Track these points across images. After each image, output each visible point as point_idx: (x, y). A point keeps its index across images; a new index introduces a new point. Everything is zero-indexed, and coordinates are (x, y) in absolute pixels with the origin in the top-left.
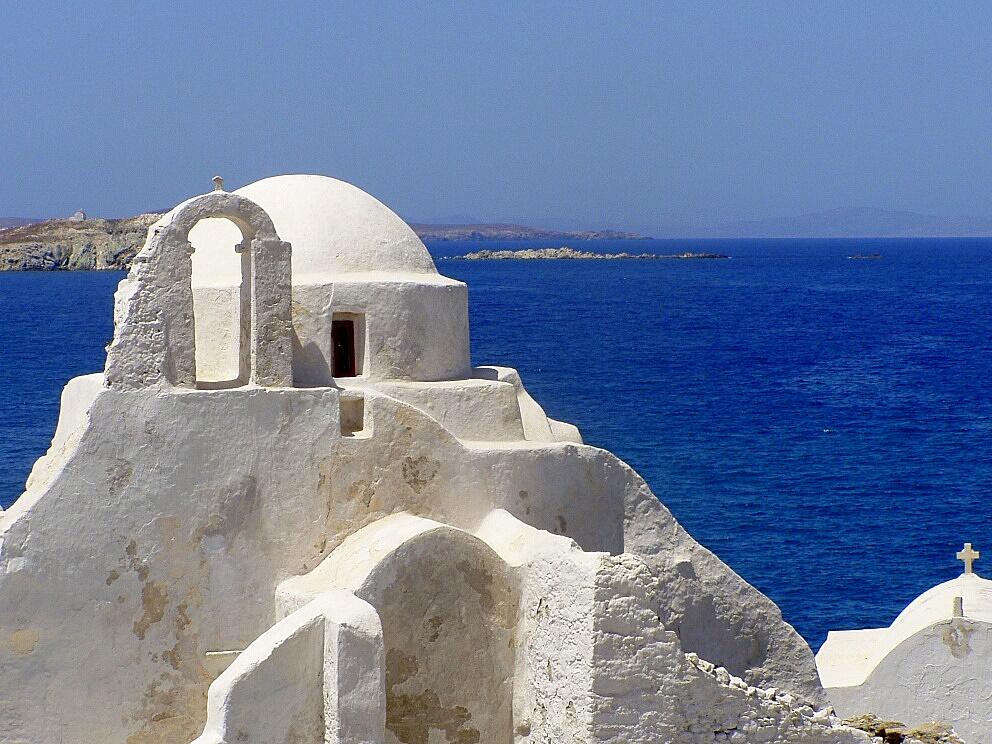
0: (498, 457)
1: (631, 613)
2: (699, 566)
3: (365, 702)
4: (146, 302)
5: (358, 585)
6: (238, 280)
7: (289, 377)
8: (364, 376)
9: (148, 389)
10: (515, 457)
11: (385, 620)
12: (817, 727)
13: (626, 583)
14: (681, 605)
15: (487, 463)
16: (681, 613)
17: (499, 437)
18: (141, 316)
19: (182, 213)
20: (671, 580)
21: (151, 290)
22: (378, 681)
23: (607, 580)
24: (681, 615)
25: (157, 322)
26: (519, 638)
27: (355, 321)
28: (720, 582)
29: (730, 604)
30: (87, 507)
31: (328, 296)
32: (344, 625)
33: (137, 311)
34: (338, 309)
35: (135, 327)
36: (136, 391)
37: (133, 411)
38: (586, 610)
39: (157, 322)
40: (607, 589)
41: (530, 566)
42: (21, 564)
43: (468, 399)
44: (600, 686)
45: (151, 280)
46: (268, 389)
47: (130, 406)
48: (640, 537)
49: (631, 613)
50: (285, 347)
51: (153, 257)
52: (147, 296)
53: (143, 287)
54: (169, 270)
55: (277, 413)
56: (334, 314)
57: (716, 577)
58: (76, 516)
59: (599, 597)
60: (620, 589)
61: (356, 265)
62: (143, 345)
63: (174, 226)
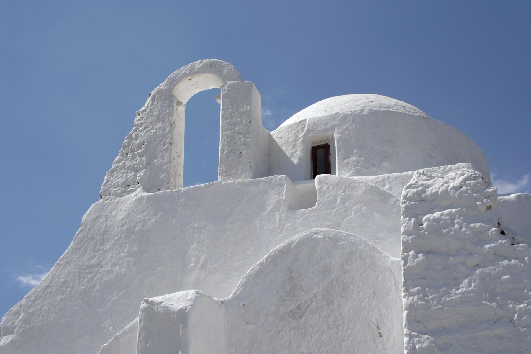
30: (69, 289)
31: (304, 128)
37: (113, 214)
47: (112, 210)
58: (59, 297)
62: (129, 168)
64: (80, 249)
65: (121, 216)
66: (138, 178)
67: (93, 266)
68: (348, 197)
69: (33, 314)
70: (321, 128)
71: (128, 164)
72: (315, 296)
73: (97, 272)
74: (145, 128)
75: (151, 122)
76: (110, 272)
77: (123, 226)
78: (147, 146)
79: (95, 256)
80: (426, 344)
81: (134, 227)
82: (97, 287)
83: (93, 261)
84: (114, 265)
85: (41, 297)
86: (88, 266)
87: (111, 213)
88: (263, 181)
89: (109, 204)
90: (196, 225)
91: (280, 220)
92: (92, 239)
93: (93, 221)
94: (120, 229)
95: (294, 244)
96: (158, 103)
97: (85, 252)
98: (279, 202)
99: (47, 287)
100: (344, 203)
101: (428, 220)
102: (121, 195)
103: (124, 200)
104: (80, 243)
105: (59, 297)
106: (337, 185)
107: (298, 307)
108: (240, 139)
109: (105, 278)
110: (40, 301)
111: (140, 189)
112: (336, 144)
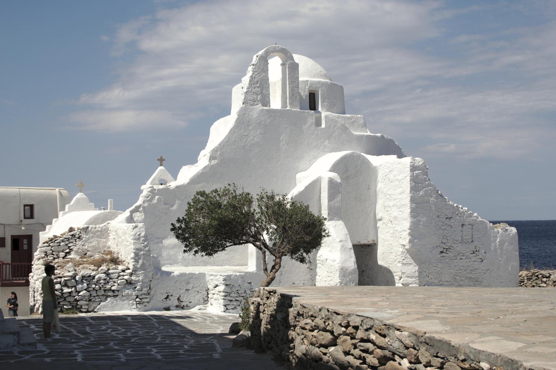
0: (363, 136)
3: (336, 205)
5: (328, 170)
6: (281, 76)
7: (299, 106)
9: (256, 107)
11: (341, 178)
12: (475, 218)
13: (419, 166)
17: (361, 131)
19: (265, 51)
21: (256, 75)
22: (340, 198)
23: (414, 165)
25: (258, 85)
26: (378, 190)
30: (237, 144)
31: (308, 84)
32: (330, 178)
33: (252, 81)
34: (311, 89)
35: (252, 86)
36: (252, 107)
37: (251, 114)
38: (406, 175)
39: (258, 85)
40: (413, 168)
41: (381, 166)
42: (216, 162)
43: (351, 119)
44: (412, 200)
45: (256, 72)
47: (250, 112)
50: (297, 97)
52: (255, 77)
53: (253, 74)
55: (188, 219)
56: (310, 90)
58: (233, 147)
61: (315, 77)
62: (254, 92)
63: (263, 55)
64: (239, 127)
65: (255, 116)
66: (259, 99)
67: (245, 136)
68: (334, 126)
69: (223, 152)
70: (315, 86)
71: (253, 91)
72: (352, 174)
73: (248, 139)
74: (258, 74)
75: (260, 72)
76: (253, 140)
77: (257, 121)
78: (260, 83)
79: (245, 131)
80: (414, 206)
81: (261, 122)
82: (248, 145)
83: (245, 134)
84: (254, 137)
85: (226, 145)
86: (243, 135)
87: (250, 113)
88: (306, 112)
89: (248, 108)
90: (284, 126)
91: (313, 130)
92: (244, 123)
93: (243, 115)
94: (255, 122)
95: (348, 156)
96: (262, 62)
97: (241, 129)
98: (312, 122)
99: (227, 141)
100: (334, 128)
101: (415, 173)
102: (253, 105)
103: (255, 108)
104: (239, 124)
105: (233, 147)
106: (332, 120)
107: (348, 176)
108: (296, 90)
109: (251, 142)
110: (225, 147)
111: (260, 105)
112: (320, 95)
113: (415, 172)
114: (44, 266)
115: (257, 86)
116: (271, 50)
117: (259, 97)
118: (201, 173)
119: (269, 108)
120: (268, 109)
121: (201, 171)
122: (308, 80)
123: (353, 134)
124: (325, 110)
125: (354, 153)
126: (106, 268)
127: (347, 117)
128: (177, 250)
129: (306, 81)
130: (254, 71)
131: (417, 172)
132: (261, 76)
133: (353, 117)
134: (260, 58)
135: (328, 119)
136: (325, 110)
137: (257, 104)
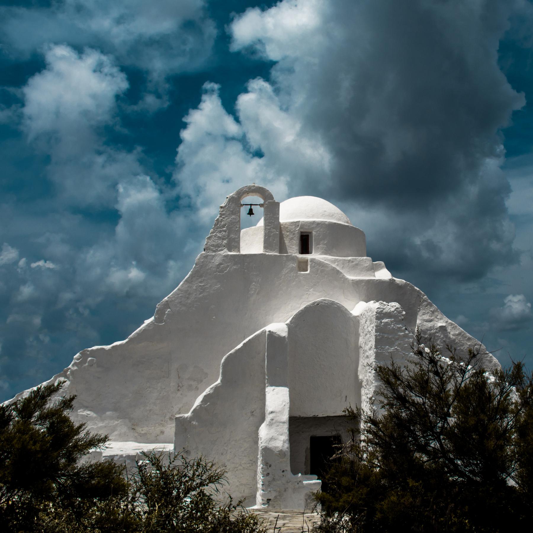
0: (361, 281)
1: (392, 326)
2: (449, 329)
4: (221, 222)
8: (313, 253)
9: (220, 252)
10: (369, 281)
11: (24, 257)
14: (442, 343)
15: (357, 283)
16: (441, 346)
18: (219, 227)
20: (437, 333)
21: (224, 218)
24: (442, 347)
25: (225, 229)
27: (310, 235)
28: (459, 334)
29: (463, 343)
31: (298, 225)
34: (302, 230)
39: (225, 229)
45: (224, 214)
46: (267, 254)
48: (424, 316)
49: (392, 326)
51: (225, 206)
54: (231, 211)
57: (457, 333)
59: (377, 318)
60: (388, 315)
63: (234, 196)
113: (383, 321)
114: (76, 425)
115: (223, 230)
116: (245, 190)
117: (225, 242)
118: (144, 330)
119: (238, 253)
120: (239, 255)
121: (143, 329)
122: (299, 221)
123: (347, 279)
124: (320, 253)
125: (325, 300)
126: (51, 437)
127: (347, 260)
128: (107, 422)
129: (297, 222)
130: (221, 214)
131: (386, 320)
132: (230, 219)
133: (355, 259)
134: (230, 200)
135: (314, 262)
136: (320, 253)
137: (222, 250)
